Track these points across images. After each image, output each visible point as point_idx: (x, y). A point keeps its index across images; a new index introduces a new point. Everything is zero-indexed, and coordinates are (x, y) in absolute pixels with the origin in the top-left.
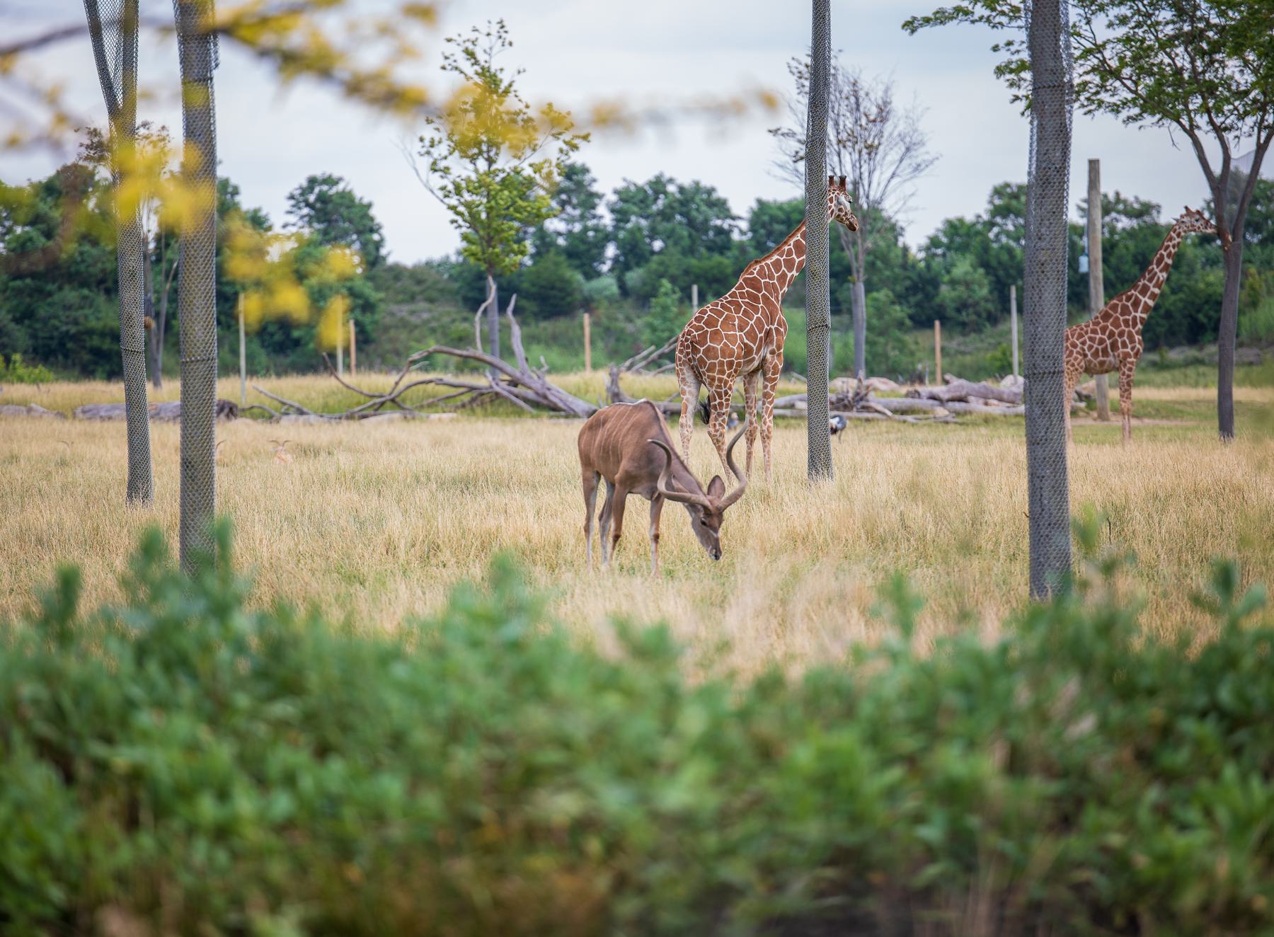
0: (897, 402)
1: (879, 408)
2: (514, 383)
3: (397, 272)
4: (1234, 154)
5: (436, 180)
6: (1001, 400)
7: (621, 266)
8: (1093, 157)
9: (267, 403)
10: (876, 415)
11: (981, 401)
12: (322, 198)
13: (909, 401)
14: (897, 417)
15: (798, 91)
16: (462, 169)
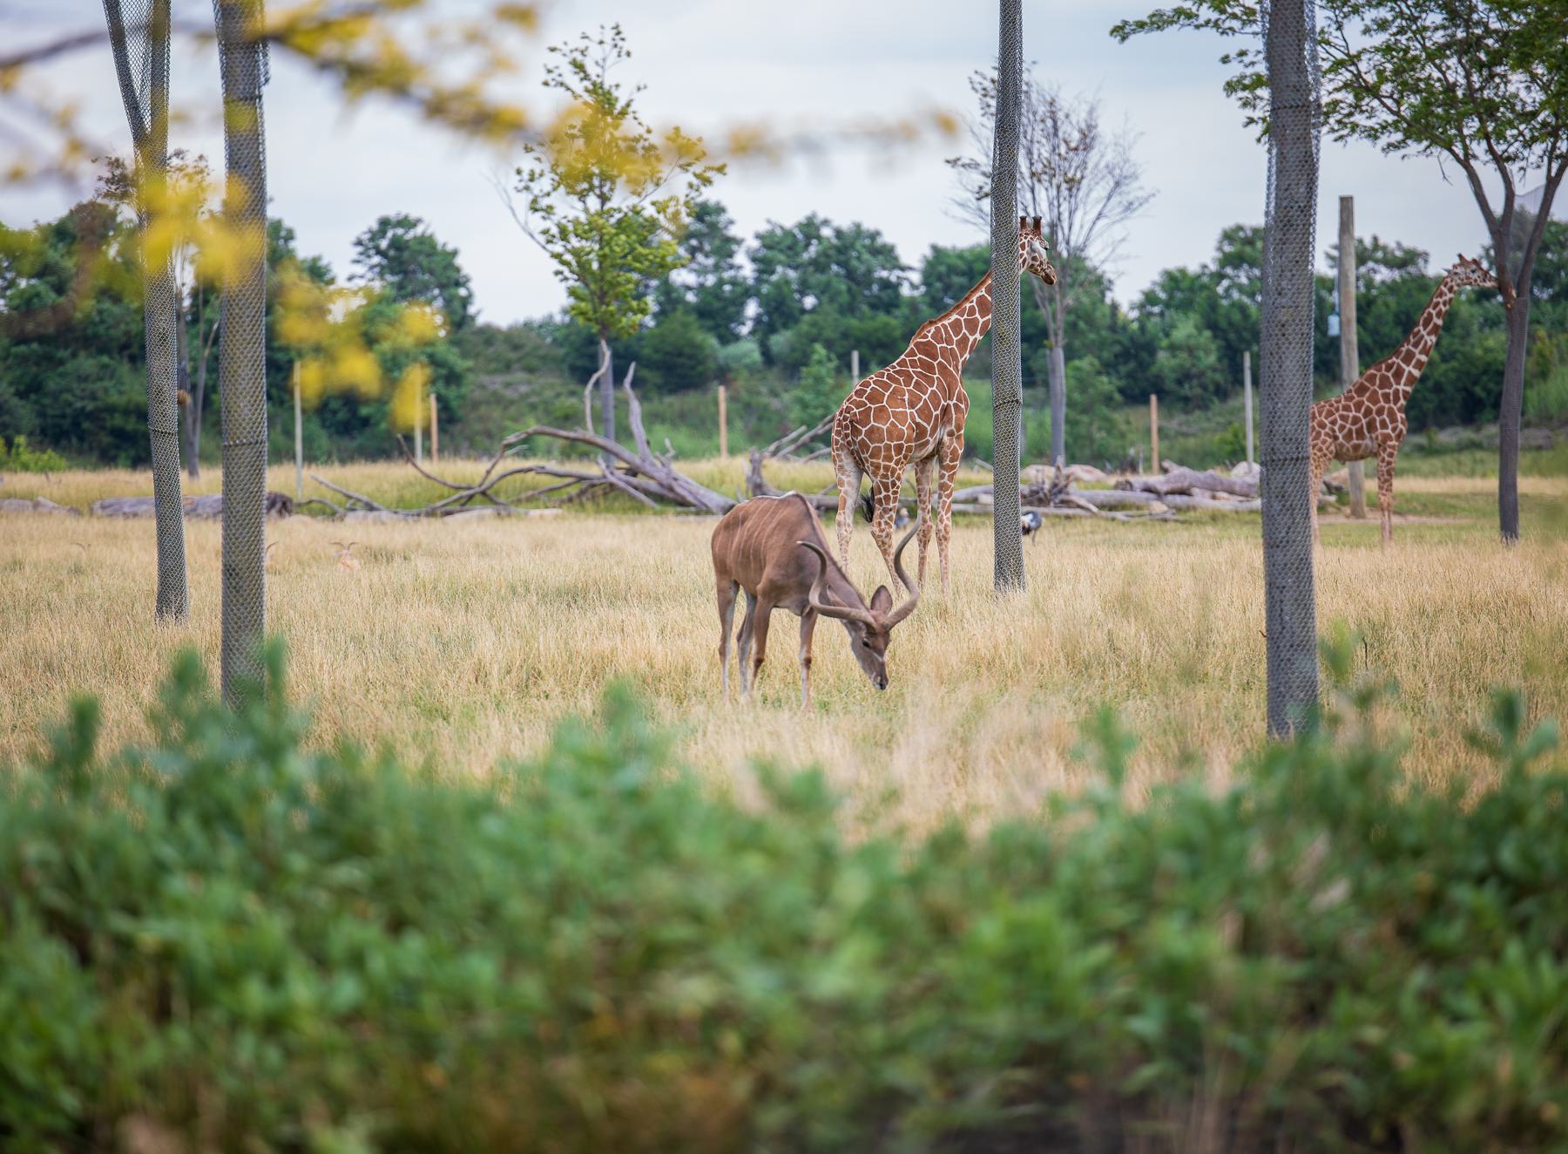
0: (1104, 495)
1: (1082, 502)
2: (633, 472)
3: (489, 335)
4: (1519, 190)
5: (537, 222)
6: (1232, 492)
7: (765, 328)
8: (1346, 193)
9: (329, 496)
10: (1079, 511)
11: (1208, 494)
12: (397, 244)
13: (1119, 494)
14: (1104, 513)
15: (983, 112)
16: (569, 208)
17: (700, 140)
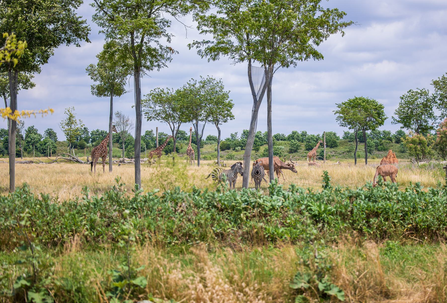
0: (129, 162)
2: (73, 158)
3: (60, 142)
4: (175, 126)
5: (63, 129)
7: (92, 142)
9: (38, 161)
12: (50, 132)
16: (66, 127)
17: (204, 84)
